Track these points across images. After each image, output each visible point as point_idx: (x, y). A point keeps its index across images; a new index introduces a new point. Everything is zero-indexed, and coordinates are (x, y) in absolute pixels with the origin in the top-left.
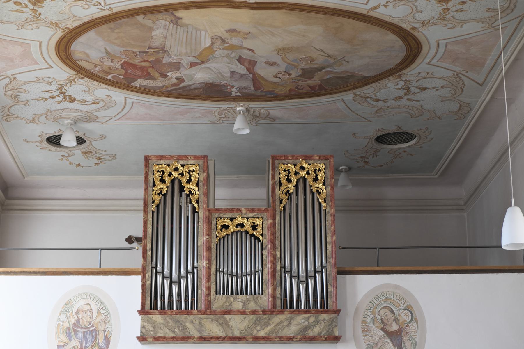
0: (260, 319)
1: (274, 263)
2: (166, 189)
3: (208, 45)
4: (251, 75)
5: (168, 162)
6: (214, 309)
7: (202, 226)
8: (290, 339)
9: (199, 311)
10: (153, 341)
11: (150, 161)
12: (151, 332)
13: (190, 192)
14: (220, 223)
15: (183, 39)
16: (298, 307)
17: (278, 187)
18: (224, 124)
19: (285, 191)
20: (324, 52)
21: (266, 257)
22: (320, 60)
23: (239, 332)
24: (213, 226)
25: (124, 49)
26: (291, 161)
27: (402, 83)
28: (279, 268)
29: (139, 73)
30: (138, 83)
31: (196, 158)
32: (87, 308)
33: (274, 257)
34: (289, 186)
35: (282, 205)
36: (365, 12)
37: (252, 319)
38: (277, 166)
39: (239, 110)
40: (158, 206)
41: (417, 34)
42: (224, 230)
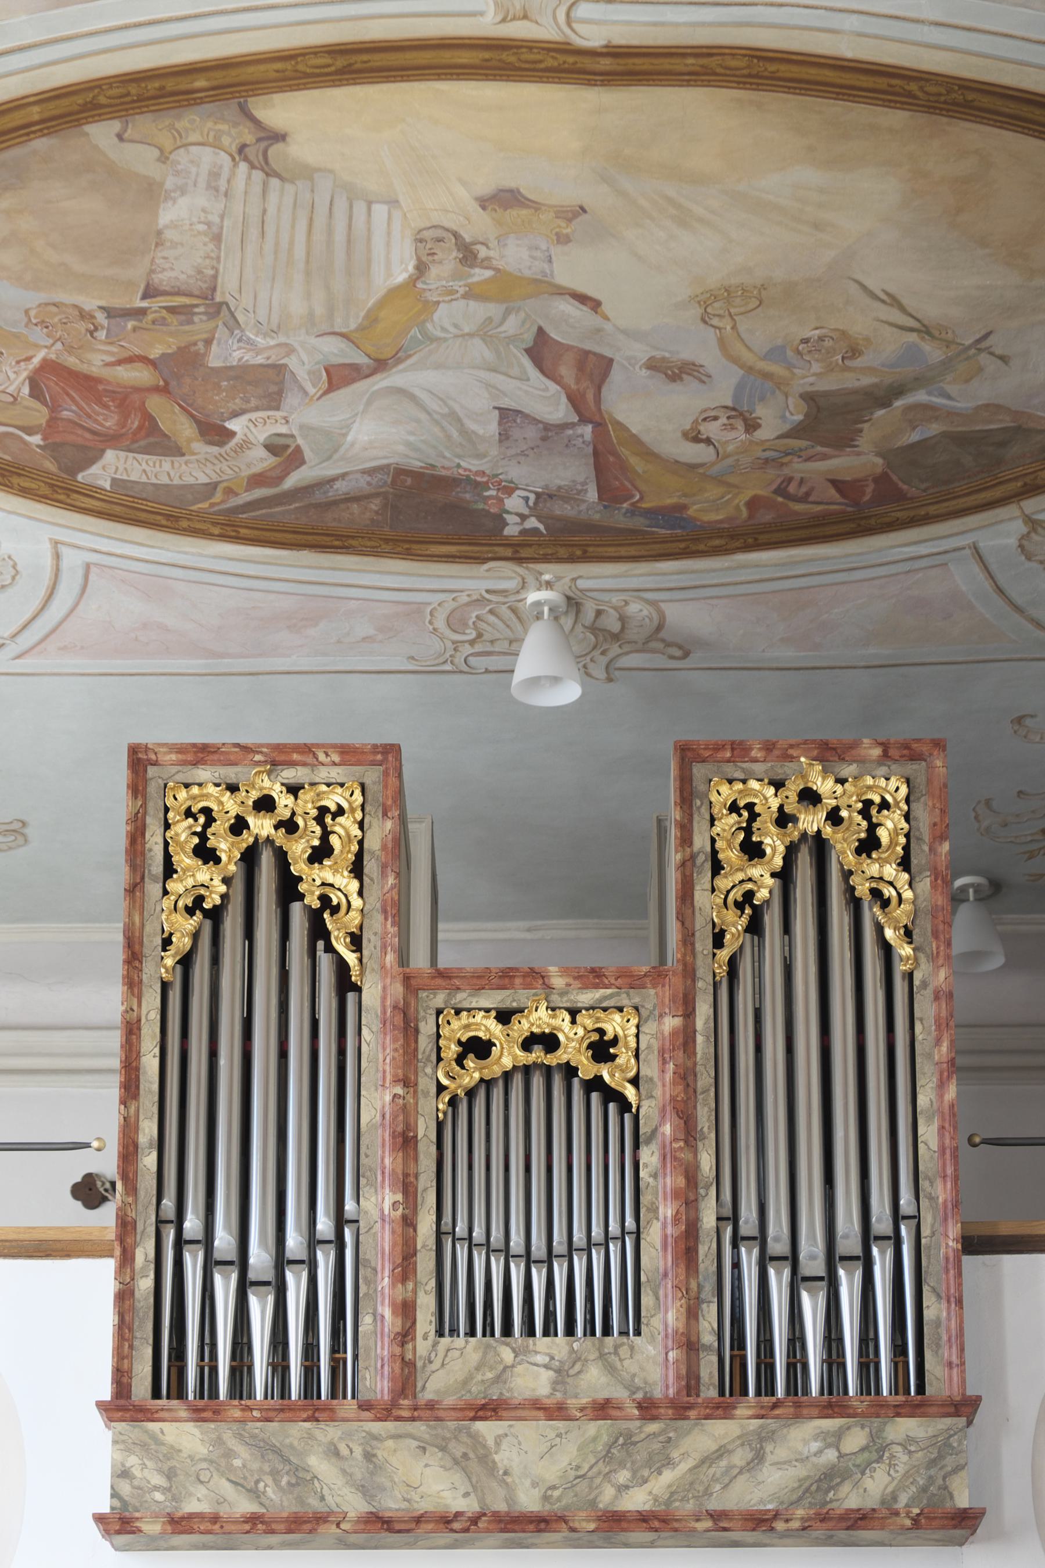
0: (629, 1441)
1: (688, 1199)
2: (223, 889)
3: (401, 278)
4: (588, 430)
6: (427, 1395)
8: (761, 1525)
9: (365, 1406)
10: (164, 1532)
11: (151, 771)
12: (158, 1496)
13: (325, 899)
14: (457, 1029)
15: (292, 243)
16: (791, 1388)
17: (703, 880)
18: (471, 671)
19: (737, 894)
20: (902, 309)
21: (655, 1176)
22: (886, 348)
23: (537, 1493)
24: (425, 1043)
25: (42, 297)
26: (759, 768)
28: (708, 1220)
29: (110, 422)
31: (349, 754)
34: (755, 872)
35: (724, 954)
37: (595, 1439)
38: (702, 788)
39: (538, 604)
40: (186, 962)
42: (470, 1062)
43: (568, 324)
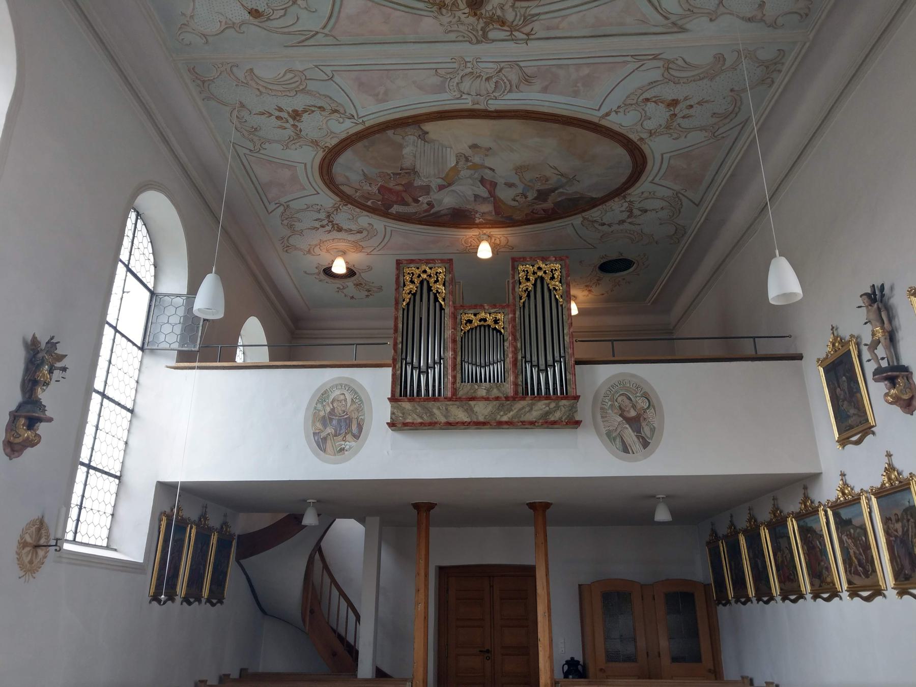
0: (503, 405)
1: (515, 353)
5: (417, 265)
7: (448, 321)
9: (445, 398)
14: (466, 317)
16: (538, 394)
24: (458, 320)
27: (626, 205)
28: (520, 357)
30: (396, 209)
31: (443, 261)
32: (342, 397)
33: (516, 348)
36: (596, 120)
40: (408, 304)
41: (645, 148)
43: (488, 175)
